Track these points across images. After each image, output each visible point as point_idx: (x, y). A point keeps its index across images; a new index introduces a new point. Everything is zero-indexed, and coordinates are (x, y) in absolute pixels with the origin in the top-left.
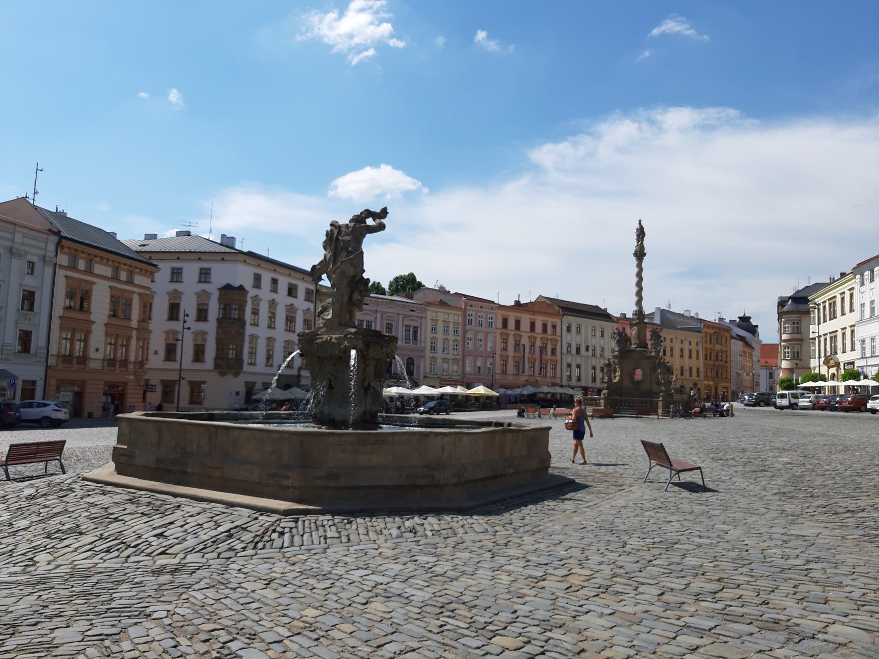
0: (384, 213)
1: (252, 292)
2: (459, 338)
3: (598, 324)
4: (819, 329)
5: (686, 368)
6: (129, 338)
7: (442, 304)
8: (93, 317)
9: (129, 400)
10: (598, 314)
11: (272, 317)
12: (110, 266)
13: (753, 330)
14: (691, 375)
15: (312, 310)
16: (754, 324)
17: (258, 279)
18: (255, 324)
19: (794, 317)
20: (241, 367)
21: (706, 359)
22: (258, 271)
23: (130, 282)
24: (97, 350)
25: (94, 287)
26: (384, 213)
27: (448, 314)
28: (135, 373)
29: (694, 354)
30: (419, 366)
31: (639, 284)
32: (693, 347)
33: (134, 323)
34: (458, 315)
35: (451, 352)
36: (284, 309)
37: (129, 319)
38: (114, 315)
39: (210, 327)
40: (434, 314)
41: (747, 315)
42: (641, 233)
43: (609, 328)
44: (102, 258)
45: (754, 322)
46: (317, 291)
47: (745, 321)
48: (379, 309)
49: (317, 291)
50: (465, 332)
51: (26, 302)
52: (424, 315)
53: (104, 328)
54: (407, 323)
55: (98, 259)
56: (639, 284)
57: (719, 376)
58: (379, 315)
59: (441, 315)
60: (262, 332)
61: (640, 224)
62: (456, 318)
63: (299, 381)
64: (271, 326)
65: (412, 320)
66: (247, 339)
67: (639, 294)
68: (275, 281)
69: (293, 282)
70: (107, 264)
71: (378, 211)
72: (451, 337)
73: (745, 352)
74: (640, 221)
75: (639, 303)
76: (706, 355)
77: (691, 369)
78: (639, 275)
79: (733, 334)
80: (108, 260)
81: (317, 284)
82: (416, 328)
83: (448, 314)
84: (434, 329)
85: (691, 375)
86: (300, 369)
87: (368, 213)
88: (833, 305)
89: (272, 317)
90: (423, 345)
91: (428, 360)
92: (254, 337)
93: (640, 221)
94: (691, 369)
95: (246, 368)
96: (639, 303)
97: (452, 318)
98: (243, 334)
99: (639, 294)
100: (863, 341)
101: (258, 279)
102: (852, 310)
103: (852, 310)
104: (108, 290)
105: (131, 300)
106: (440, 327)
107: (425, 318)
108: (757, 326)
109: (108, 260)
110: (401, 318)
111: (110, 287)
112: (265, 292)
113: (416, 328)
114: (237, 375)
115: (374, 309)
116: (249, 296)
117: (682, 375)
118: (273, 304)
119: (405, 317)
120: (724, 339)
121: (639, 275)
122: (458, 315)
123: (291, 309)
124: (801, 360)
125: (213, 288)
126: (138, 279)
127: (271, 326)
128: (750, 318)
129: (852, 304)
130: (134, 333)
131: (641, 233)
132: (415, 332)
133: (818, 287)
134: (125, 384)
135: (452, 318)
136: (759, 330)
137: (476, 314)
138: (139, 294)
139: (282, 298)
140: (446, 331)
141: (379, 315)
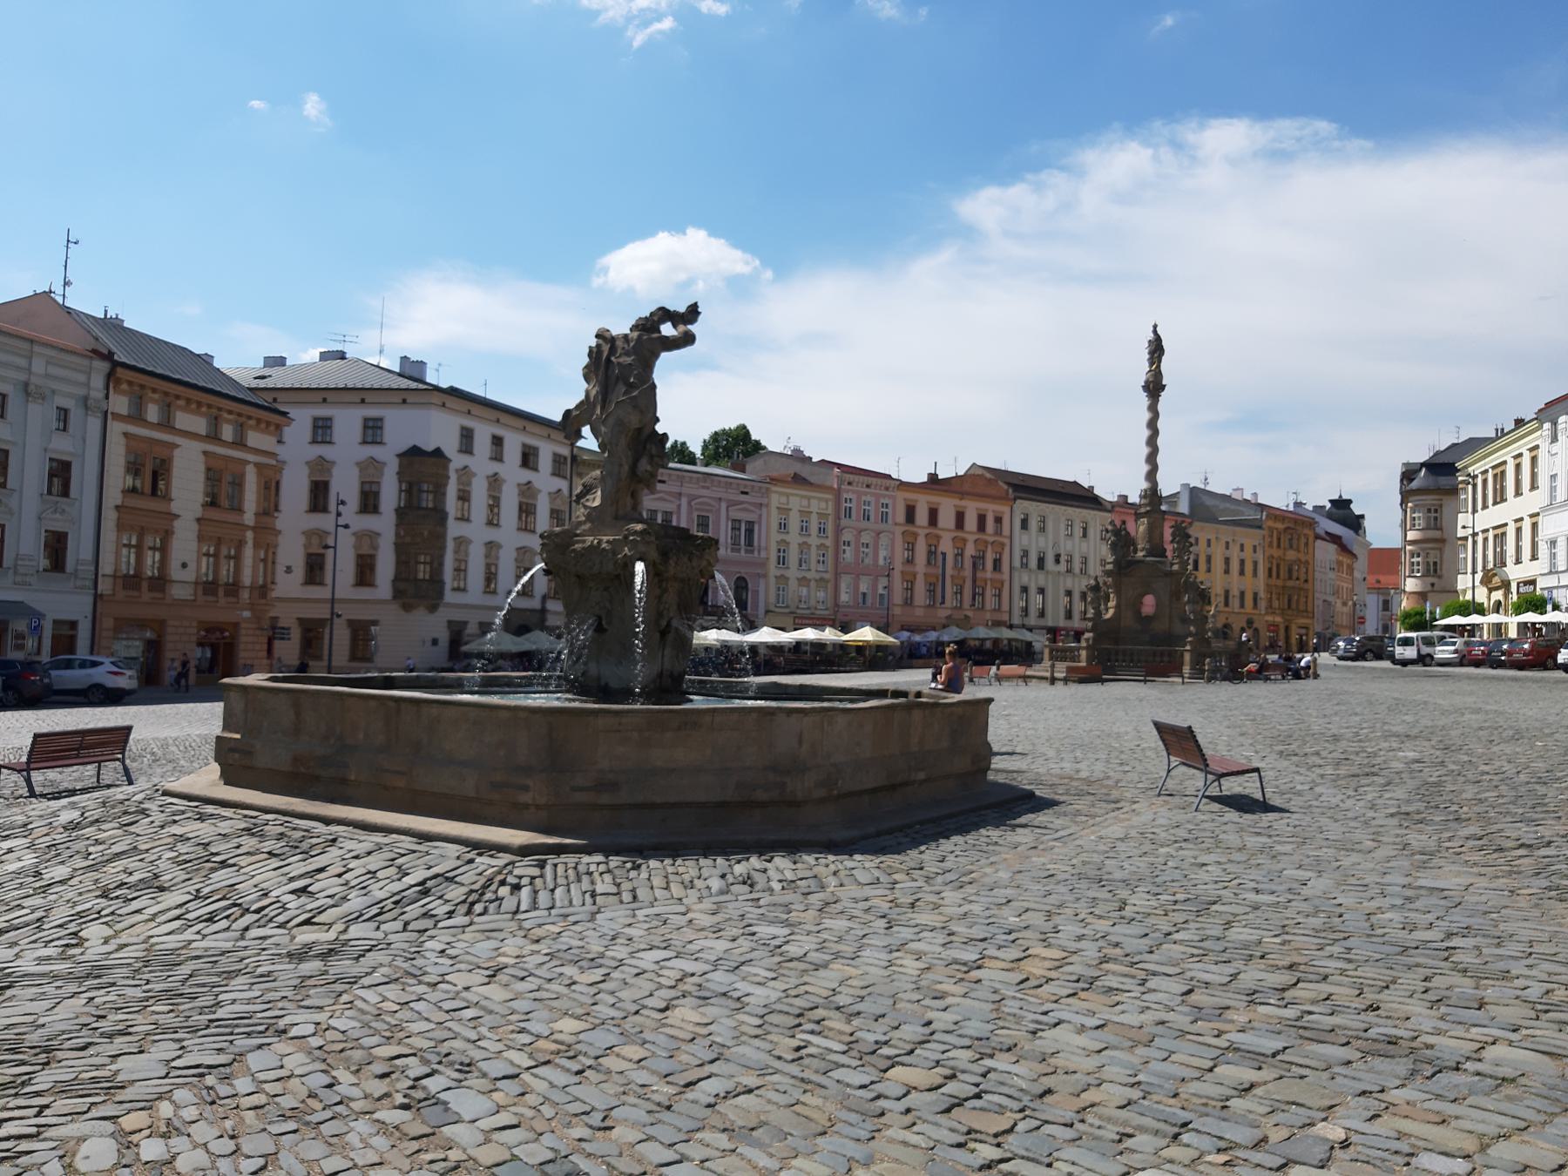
0: (693, 313)
1: (457, 461)
2: (828, 542)
3: (1078, 514)
5: (1235, 592)
6: (240, 544)
7: (798, 480)
8: (175, 507)
11: (495, 505)
13: (1356, 523)
14: (1242, 606)
15: (566, 491)
16: (1357, 513)
17: (467, 436)
18: (464, 519)
19: (1430, 499)
20: (441, 594)
21: (1270, 575)
22: (468, 422)
23: (240, 443)
26: (693, 313)
31: (1152, 442)
32: (1248, 554)
33: (249, 518)
34: (827, 501)
36: (516, 491)
37: (239, 510)
38: (212, 502)
39: (384, 524)
42: (1156, 349)
44: (188, 401)
45: (1356, 509)
46: (574, 458)
48: (684, 490)
49: (574, 458)
50: (838, 530)
52: (764, 501)
53: (195, 527)
55: (181, 403)
56: (1152, 442)
59: (796, 500)
61: (1155, 331)
62: (823, 505)
66: (450, 546)
70: (197, 412)
71: (682, 309)
72: (814, 540)
73: (1340, 563)
74: (1155, 327)
76: (1270, 570)
77: (1242, 594)
78: (1153, 425)
79: (1320, 531)
81: (572, 445)
82: (750, 524)
84: (783, 526)
85: (1242, 606)
86: (544, 598)
87: (664, 314)
88: (1500, 477)
89: (495, 505)
90: (763, 554)
91: (772, 581)
92: (462, 542)
93: (1155, 327)
94: (1242, 594)
95: (449, 597)
97: (815, 506)
100: (1553, 543)
101: (467, 436)
102: (1534, 487)
103: (1534, 487)
104: (202, 458)
105: (243, 475)
106: (794, 523)
108: (1362, 516)
109: (199, 404)
110: (724, 505)
112: (480, 462)
113: (750, 524)
114: (433, 608)
116: (453, 467)
118: (495, 481)
119: (731, 504)
120: (1303, 540)
121: (1153, 425)
122: (827, 501)
123: (527, 490)
124: (1440, 577)
125: (388, 454)
126: (255, 439)
128: (1350, 502)
130: (249, 535)
131: (1156, 349)
132: (750, 532)
133: (1474, 445)
134: (236, 625)
135: (815, 506)
136: (1367, 523)
137: (859, 498)
138: (256, 465)
140: (804, 530)
141: (684, 501)
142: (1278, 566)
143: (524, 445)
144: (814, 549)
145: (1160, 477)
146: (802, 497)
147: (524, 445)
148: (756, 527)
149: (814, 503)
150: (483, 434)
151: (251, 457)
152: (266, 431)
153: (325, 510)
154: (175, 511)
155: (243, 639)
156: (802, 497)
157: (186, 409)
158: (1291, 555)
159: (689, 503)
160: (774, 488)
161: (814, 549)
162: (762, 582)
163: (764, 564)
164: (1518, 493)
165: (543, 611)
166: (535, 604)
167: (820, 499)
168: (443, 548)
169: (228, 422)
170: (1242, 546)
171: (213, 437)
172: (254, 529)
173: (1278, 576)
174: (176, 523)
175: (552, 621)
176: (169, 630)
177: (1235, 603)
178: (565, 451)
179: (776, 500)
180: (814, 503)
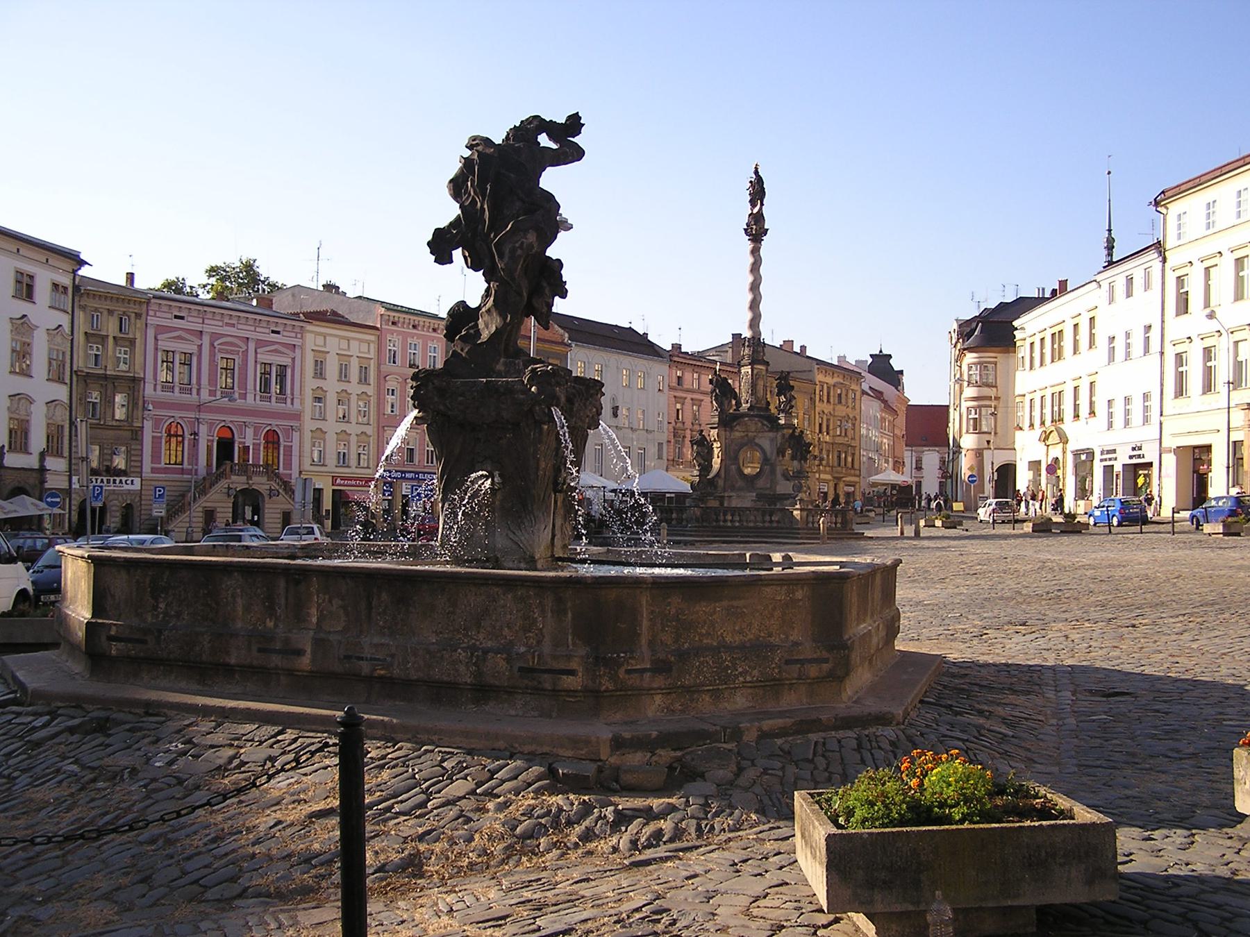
0: (575, 124)
2: (371, 390)
4: (1029, 381)
7: (334, 318)
13: (894, 378)
26: (575, 124)
30: (289, 449)
31: (755, 287)
35: (353, 420)
40: (320, 340)
41: (885, 352)
42: (758, 191)
45: (896, 364)
46: (76, 288)
47: (881, 365)
48: (207, 329)
50: (382, 377)
56: (755, 287)
57: (843, 463)
59: (331, 341)
61: (756, 172)
62: (364, 347)
63: (43, 481)
65: (276, 351)
67: (755, 305)
69: (28, 268)
71: (561, 120)
72: (354, 388)
73: (883, 419)
75: (755, 323)
79: (865, 387)
81: (74, 272)
82: (282, 369)
86: (42, 456)
87: (536, 125)
88: (1057, 337)
91: (307, 435)
96: (755, 323)
97: (355, 349)
99: (755, 305)
102: (1092, 344)
103: (1092, 344)
106: (332, 368)
107: (302, 347)
108: (901, 372)
110: (252, 346)
113: (282, 369)
115: (198, 327)
119: (260, 343)
120: (851, 395)
129: (1092, 336)
131: (758, 191)
132: (282, 377)
133: (1025, 305)
135: (355, 349)
136: (906, 379)
137: (404, 341)
140: (344, 375)
142: (828, 420)
143: (19, 273)
145: (763, 327)
147: (19, 273)
148: (289, 371)
153: (1077, 454)
158: (841, 410)
160: (309, 327)
162: (296, 435)
163: (297, 416)
164: (1076, 350)
165: (42, 470)
166: (32, 461)
175: (52, 482)
178: (66, 280)
180: (354, 344)
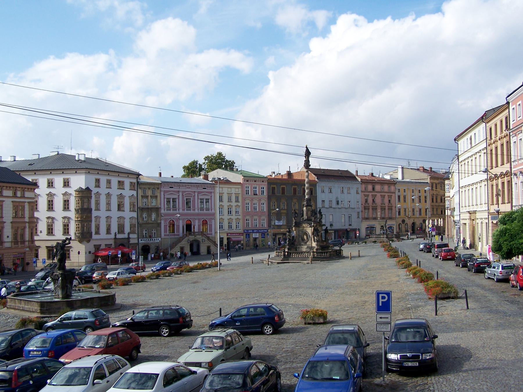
1: (94, 190)
3: (346, 184)
5: (417, 209)
6: (25, 227)
8: (4, 220)
9: (27, 259)
10: (345, 176)
11: (109, 204)
12: (11, 190)
14: (420, 214)
15: (135, 195)
17: (98, 181)
18: (98, 209)
20: (91, 236)
21: (433, 201)
22: (98, 177)
23: (23, 197)
24: (8, 237)
25: (4, 203)
27: (231, 188)
28: (29, 247)
29: (423, 199)
30: (211, 226)
33: (27, 219)
34: (238, 188)
36: (116, 198)
37: (24, 218)
38: (16, 216)
39: (72, 214)
43: (354, 187)
44: (7, 187)
46: (138, 182)
48: (180, 190)
49: (138, 182)
51: (143, 351)
52: (212, 191)
53: (10, 225)
54: (200, 197)
55: (5, 188)
58: (181, 194)
60: (103, 213)
62: (237, 190)
63: (129, 242)
64: (109, 210)
66: (93, 219)
68: (109, 182)
70: (10, 189)
72: (234, 204)
76: (433, 199)
77: (420, 210)
80: (10, 187)
83: (231, 188)
84: (221, 200)
85: (420, 214)
86: (129, 234)
89: (109, 204)
90: (213, 211)
92: (97, 217)
94: (420, 210)
95: (94, 236)
98: (91, 217)
101: (98, 181)
104: (12, 203)
105: (24, 206)
106: (225, 198)
107: (214, 192)
109: (10, 187)
110: (196, 194)
111: (12, 202)
112: (103, 190)
114: (89, 241)
115: (178, 190)
116: (93, 193)
117: (414, 214)
118: (108, 195)
119: (199, 193)
122: (238, 188)
123: (121, 197)
125: (72, 191)
126: (28, 194)
127: (109, 210)
130: (27, 225)
134: (25, 253)
138: (29, 203)
139: (115, 191)
140: (230, 200)
141: (181, 194)
144: (234, 220)
146: (228, 188)
149: (233, 190)
150: (103, 179)
151: (27, 200)
152: (31, 191)
154: (4, 221)
155: (27, 257)
156: (228, 188)
157: (6, 189)
159: (183, 195)
161: (234, 220)
162: (213, 221)
165: (129, 238)
167: (235, 188)
168: (91, 221)
169: (19, 190)
170: (419, 190)
171: (15, 195)
172: (29, 222)
173: (437, 202)
174: (5, 224)
176: (5, 257)
177: (417, 214)
178: (135, 181)
179: (217, 190)
